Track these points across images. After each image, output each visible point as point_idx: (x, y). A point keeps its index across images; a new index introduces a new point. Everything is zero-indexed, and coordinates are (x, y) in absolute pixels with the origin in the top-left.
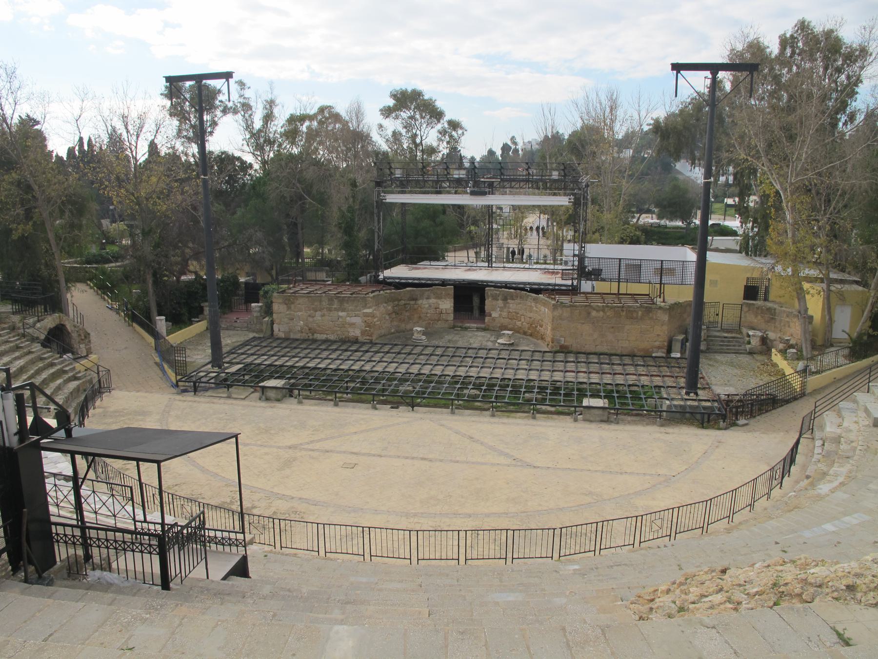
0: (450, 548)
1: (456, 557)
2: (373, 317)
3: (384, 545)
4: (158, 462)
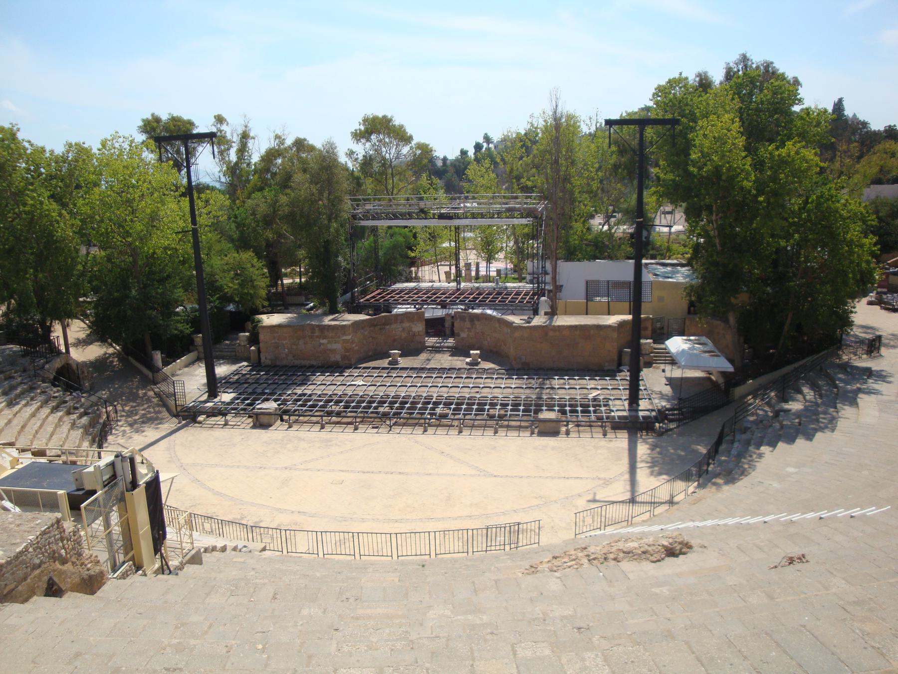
0: (423, 546)
1: (428, 553)
2: (353, 342)
3: (371, 546)
4: (633, 501)
